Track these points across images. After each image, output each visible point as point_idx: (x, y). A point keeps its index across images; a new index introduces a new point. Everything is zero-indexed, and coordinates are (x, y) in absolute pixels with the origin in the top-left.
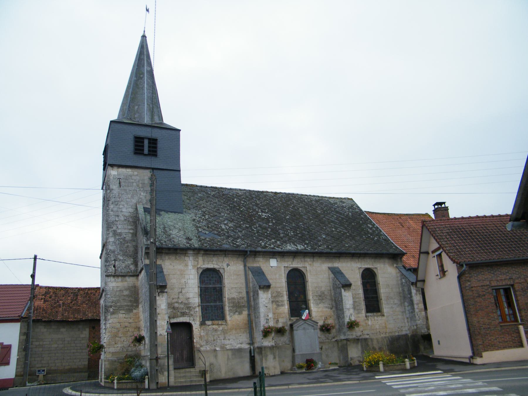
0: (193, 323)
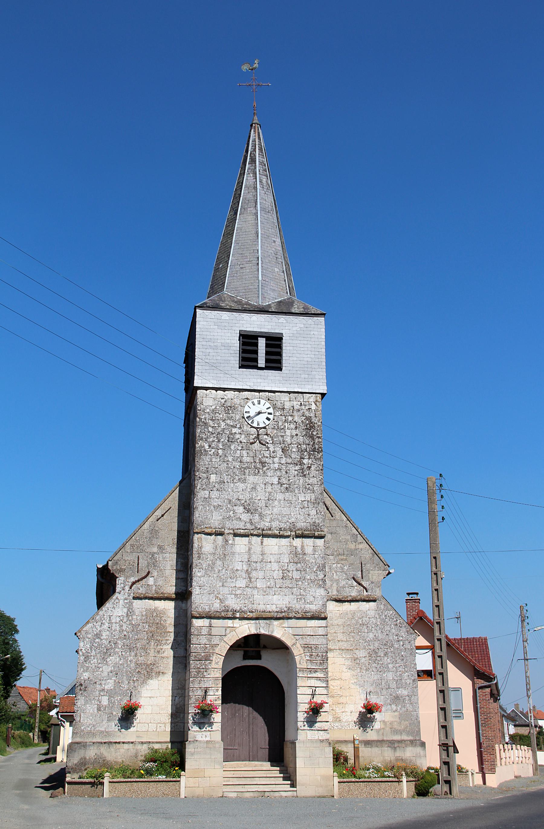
0: (232, 638)
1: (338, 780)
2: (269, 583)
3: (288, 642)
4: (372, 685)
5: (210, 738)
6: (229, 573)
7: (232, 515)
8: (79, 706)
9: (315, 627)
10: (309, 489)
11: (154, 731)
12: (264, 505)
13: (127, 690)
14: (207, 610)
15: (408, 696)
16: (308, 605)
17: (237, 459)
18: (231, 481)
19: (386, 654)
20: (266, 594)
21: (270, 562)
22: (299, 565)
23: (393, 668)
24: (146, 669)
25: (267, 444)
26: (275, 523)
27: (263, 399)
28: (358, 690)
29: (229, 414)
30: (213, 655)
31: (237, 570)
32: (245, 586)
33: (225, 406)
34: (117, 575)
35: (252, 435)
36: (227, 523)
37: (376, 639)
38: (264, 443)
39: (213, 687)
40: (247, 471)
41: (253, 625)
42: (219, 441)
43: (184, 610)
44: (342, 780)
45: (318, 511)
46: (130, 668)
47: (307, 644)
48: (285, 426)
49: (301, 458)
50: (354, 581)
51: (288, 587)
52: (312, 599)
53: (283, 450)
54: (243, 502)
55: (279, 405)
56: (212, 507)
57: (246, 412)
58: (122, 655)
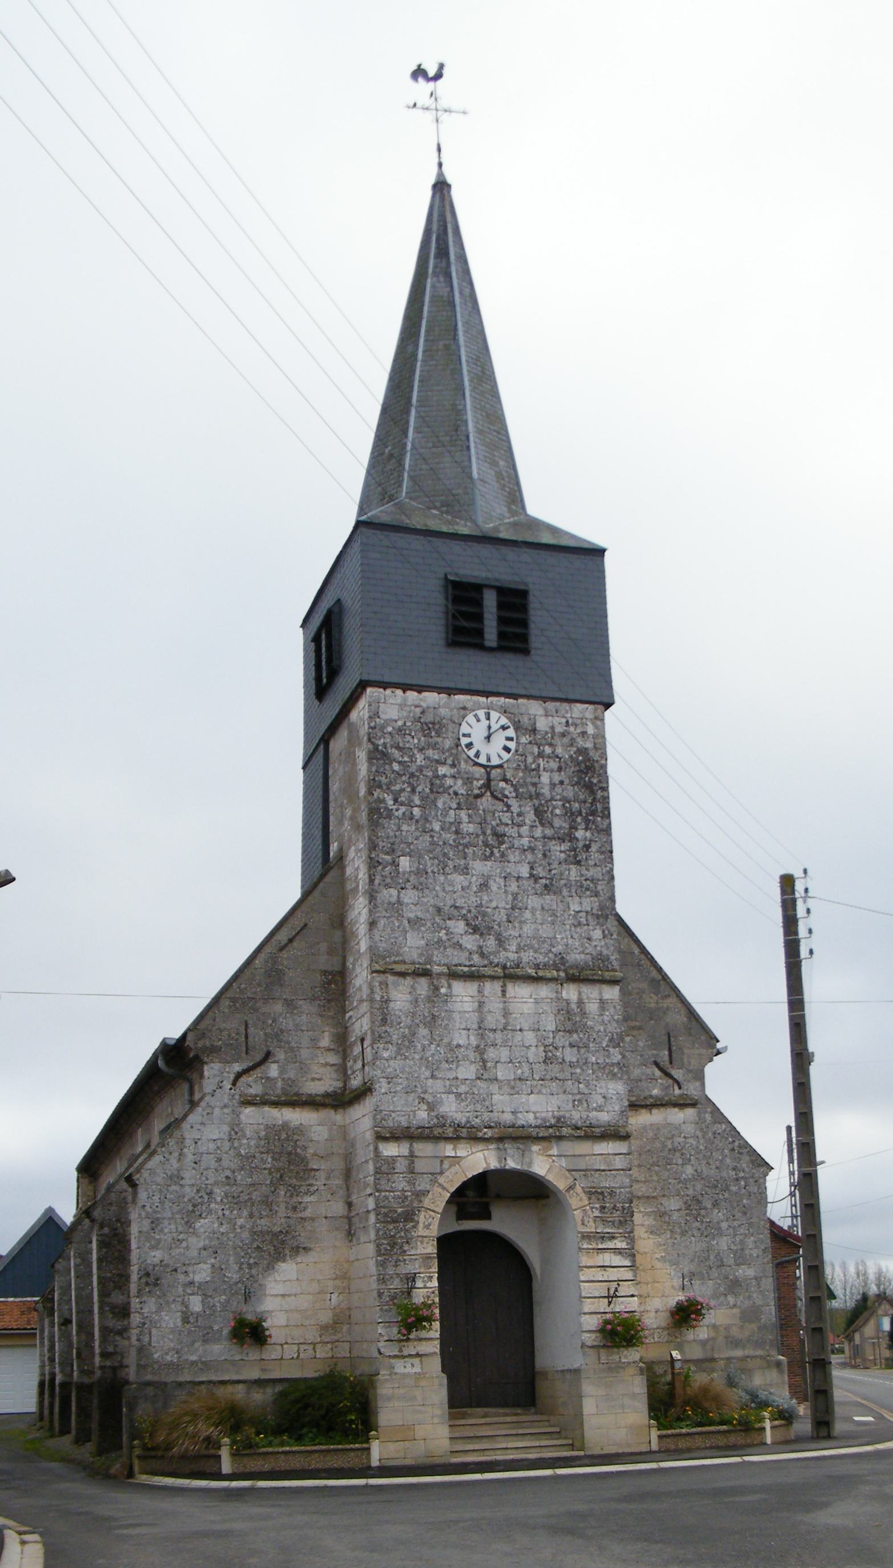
0: (454, 1179)
1: (659, 1433)
2: (519, 1071)
3: (559, 1182)
4: (692, 1261)
5: (421, 1368)
6: (443, 1052)
7: (444, 938)
8: (146, 1315)
9: (608, 1154)
10: (587, 889)
11: (292, 1358)
12: (505, 918)
13: (238, 1283)
14: (405, 1124)
15: (756, 1278)
16: (594, 1113)
17: (450, 828)
18: (439, 870)
19: (716, 1204)
20: (514, 1092)
21: (521, 1030)
22: (575, 1036)
23: (727, 1229)
24: (271, 1242)
25: (505, 800)
26: (527, 954)
27: (495, 710)
28: (669, 1272)
29: (431, 737)
30: (419, 1211)
31: (459, 1046)
32: (474, 1077)
33: (422, 720)
34: (205, 1059)
35: (478, 780)
36: (436, 952)
37: (698, 1176)
38: (500, 796)
39: (422, 1273)
40: (470, 851)
41: (493, 1152)
42: (413, 791)
43: (340, 1126)
44: (664, 1432)
45: (607, 932)
46: (242, 1241)
47: (594, 1188)
48: (539, 765)
49: (571, 828)
50: (656, 1069)
51: (556, 1078)
52: (600, 1100)
53: (539, 813)
54: (464, 912)
55: (525, 721)
56: (406, 922)
57: (464, 735)
58: (224, 1215)
